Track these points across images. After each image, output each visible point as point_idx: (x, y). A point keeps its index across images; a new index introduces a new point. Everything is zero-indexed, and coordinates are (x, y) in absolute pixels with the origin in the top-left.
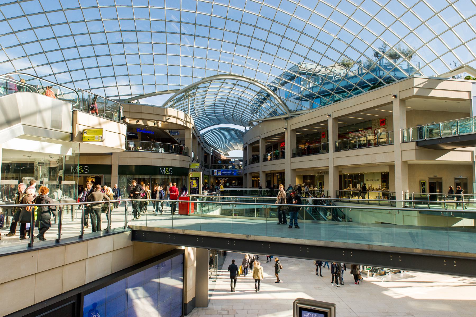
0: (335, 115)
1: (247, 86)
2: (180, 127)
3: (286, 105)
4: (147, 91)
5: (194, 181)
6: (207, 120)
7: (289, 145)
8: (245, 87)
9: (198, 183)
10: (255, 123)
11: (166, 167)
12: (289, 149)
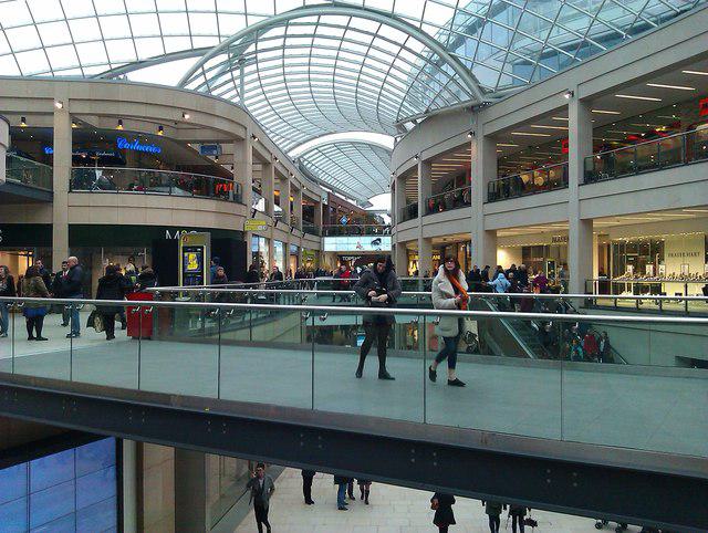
0: (585, 92)
1: (283, 33)
2: (221, 137)
3: (473, 77)
4: (149, 49)
5: (192, 256)
6: (335, 115)
7: (481, 172)
8: (281, 37)
9: (200, 260)
10: (410, 126)
11: (184, 228)
12: (480, 182)
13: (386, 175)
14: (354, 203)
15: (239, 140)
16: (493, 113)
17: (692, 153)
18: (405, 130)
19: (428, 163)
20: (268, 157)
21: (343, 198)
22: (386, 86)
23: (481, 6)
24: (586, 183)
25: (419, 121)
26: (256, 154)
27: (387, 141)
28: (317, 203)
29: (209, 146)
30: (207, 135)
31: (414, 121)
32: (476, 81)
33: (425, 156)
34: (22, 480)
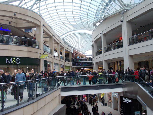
2: (31, 25)
13: (90, 43)
14: (81, 53)
15: (38, 26)
16: (129, 13)
17: (152, 38)
18: (96, 26)
19: (105, 35)
20: (51, 35)
21: (78, 51)
22: (90, 9)
23: (59, 96)
24: (105, 52)
25: (101, 21)
26: (45, 32)
27: (91, 33)
28: (70, 52)
29: (29, 29)
30: (27, 25)
31: (100, 22)
32: (123, 2)
33: (104, 33)
34: (23, 110)
